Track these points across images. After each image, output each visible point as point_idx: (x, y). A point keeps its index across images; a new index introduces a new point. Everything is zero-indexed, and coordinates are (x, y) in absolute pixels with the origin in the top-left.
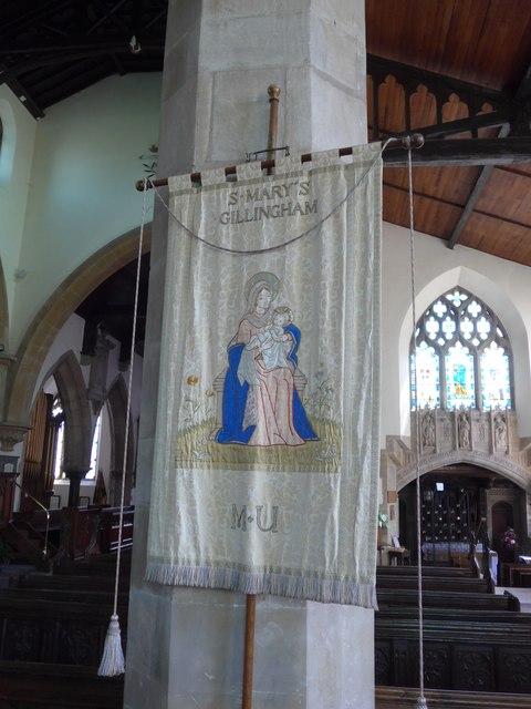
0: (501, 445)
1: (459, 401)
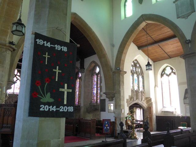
0: (143, 99)
1: (136, 88)
